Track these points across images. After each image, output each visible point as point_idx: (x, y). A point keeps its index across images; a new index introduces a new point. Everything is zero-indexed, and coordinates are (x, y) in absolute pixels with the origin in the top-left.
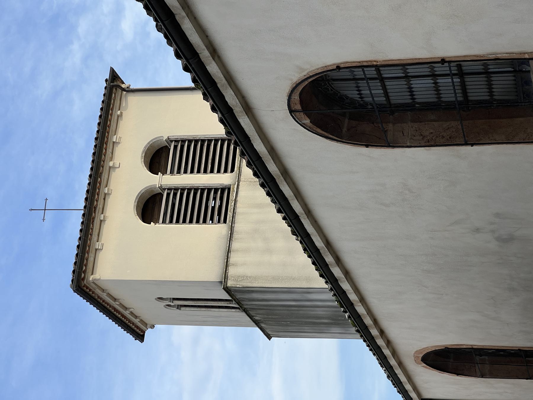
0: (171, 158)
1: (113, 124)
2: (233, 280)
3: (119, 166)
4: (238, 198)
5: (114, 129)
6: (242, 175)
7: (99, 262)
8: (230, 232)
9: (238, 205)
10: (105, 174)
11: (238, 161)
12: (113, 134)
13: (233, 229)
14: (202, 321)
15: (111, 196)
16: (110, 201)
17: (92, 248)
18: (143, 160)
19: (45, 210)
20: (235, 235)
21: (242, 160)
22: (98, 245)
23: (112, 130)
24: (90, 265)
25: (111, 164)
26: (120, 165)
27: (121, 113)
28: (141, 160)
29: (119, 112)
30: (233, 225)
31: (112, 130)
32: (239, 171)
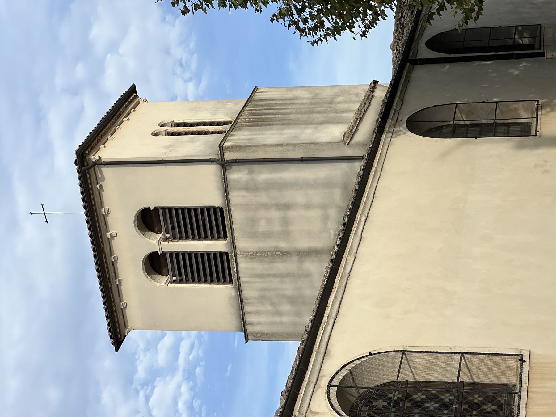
0: (162, 220)
1: (97, 199)
2: (253, 336)
3: (117, 235)
4: (239, 269)
5: (99, 203)
6: (237, 249)
7: (127, 315)
8: (240, 300)
10: (106, 246)
11: (229, 231)
12: (100, 207)
13: (241, 295)
15: (118, 261)
17: (115, 291)
18: (137, 228)
19: (45, 213)
20: (245, 301)
21: (220, 157)
23: (98, 205)
24: (121, 322)
25: (108, 235)
26: (116, 234)
27: (101, 186)
28: (135, 228)
29: (98, 186)
30: (241, 293)
31: (98, 205)
32: (234, 247)
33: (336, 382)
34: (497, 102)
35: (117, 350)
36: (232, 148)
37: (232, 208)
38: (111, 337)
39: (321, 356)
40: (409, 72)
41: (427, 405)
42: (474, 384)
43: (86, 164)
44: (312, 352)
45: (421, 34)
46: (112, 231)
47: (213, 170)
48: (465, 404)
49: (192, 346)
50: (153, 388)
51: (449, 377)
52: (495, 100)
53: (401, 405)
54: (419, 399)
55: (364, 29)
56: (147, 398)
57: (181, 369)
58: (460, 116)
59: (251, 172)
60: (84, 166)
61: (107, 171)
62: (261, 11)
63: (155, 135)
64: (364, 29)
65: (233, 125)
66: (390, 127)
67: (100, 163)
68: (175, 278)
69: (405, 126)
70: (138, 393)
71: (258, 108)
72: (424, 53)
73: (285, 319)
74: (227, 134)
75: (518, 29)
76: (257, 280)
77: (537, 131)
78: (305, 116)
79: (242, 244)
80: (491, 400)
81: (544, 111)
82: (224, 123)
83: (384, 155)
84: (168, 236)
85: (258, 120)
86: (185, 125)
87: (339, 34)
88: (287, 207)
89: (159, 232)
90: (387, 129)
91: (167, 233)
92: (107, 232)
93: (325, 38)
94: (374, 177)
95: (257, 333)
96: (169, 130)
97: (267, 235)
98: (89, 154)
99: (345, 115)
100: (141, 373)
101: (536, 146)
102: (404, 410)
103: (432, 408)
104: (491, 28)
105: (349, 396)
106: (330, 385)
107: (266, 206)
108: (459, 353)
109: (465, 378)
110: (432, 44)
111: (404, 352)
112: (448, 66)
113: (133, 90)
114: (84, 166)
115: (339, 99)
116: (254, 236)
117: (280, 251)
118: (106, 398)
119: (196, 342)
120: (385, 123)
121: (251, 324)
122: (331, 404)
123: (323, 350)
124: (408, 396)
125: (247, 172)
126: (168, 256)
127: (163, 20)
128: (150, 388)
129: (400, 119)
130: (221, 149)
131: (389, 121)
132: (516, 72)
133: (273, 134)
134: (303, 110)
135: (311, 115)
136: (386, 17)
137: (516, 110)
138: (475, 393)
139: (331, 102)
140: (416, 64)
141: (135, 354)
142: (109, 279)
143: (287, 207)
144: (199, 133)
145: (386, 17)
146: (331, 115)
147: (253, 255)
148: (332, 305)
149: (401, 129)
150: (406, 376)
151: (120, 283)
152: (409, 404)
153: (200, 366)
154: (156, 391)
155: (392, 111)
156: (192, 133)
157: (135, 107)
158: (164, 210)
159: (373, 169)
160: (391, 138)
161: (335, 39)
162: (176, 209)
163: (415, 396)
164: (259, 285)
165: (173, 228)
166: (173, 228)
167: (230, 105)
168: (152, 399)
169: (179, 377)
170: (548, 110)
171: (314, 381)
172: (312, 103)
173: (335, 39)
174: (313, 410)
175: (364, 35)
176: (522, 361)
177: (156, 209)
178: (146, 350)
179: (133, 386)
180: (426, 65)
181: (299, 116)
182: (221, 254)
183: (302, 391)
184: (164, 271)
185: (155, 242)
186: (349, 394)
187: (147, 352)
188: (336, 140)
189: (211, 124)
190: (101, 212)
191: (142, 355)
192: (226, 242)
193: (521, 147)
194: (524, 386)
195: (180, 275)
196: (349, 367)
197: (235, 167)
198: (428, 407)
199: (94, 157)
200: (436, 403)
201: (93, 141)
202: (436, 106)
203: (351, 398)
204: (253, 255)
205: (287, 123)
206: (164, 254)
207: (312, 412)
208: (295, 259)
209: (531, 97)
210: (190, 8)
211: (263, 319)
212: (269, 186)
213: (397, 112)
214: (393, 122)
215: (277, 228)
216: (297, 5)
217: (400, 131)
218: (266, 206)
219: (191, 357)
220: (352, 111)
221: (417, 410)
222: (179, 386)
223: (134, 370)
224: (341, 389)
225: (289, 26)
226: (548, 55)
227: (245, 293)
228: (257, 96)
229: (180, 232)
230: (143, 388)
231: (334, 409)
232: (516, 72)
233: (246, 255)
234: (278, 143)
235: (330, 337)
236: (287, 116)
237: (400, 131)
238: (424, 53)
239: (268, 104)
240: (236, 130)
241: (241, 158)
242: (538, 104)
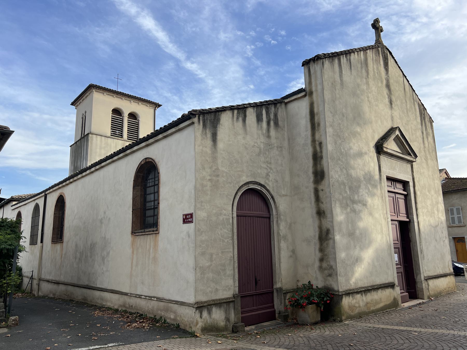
9: (117, 140)
16: (120, 100)
20: (106, 138)
22: (105, 94)
25: (132, 101)
27: (148, 107)
29: (148, 106)
46: (133, 103)
73: (98, 150)
95: (92, 138)
151: (113, 97)
160: (195, 255)
208: (225, 305)
211: (99, 142)
233: (124, 144)
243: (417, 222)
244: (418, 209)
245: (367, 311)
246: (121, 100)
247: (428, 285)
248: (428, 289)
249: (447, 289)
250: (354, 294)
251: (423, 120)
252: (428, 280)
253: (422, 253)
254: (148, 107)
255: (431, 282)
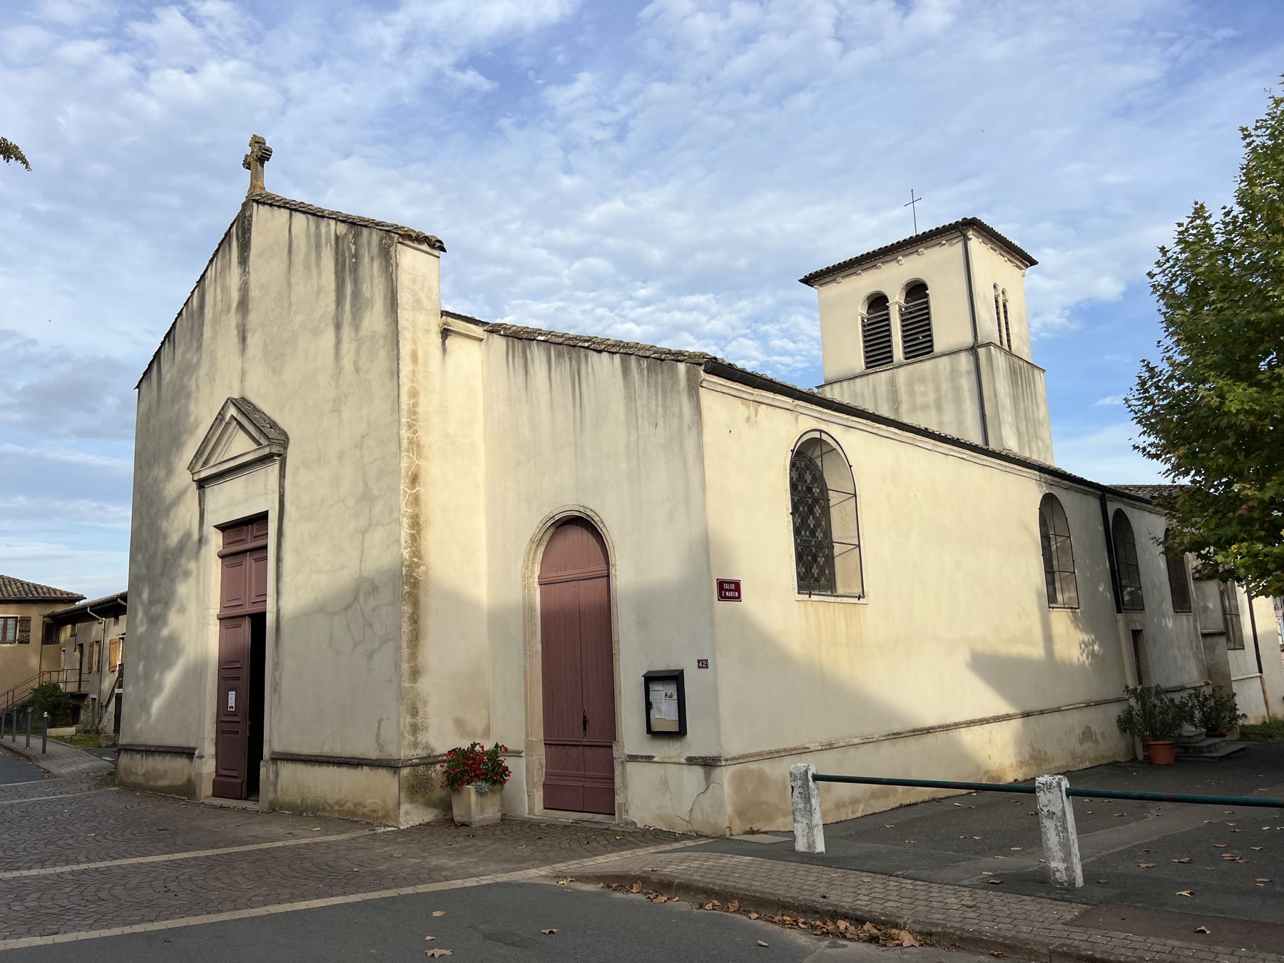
4: (879, 373)
9: (874, 375)
14: (551, 386)
16: (854, 278)
20: (852, 381)
22: (840, 279)
24: (824, 281)
27: (945, 244)
33: (824, 437)
34: (1074, 572)
35: (801, 281)
36: (989, 354)
37: (933, 361)
38: (811, 274)
39: (845, 423)
40: (1093, 494)
41: (811, 517)
42: (833, 558)
43: (964, 228)
44: (848, 414)
45: (1126, 504)
47: (968, 340)
48: (816, 550)
49: (788, 366)
50: (752, 339)
51: (836, 535)
52: (1076, 571)
53: (809, 495)
54: (815, 511)
55: (1141, 447)
56: (744, 336)
57: (770, 359)
58: (1060, 540)
59: (968, 373)
60: (962, 226)
61: (959, 247)
62: (1158, 346)
63: (995, 287)
64: (1141, 447)
65: (1009, 353)
66: (1045, 478)
67: (966, 239)
68: (866, 320)
69: (1047, 492)
70: (749, 327)
71: (1026, 374)
72: (1112, 507)
74: (1000, 348)
75: (1138, 590)
76: (871, 389)
77: (1053, 608)
78: (1023, 416)
79: (902, 374)
80: (822, 572)
81: (1071, 614)
82: (1009, 346)
83: (1020, 473)
84: (903, 309)
85: (1015, 374)
86: (1005, 312)
87: (1137, 423)
88: (939, 407)
89: (906, 302)
90: (1043, 475)
91: (906, 308)
92: (903, 256)
93: (1132, 410)
94: (1001, 465)
96: (999, 298)
97: (912, 394)
98: (973, 229)
99: (1027, 450)
100: (763, 328)
101: (1041, 607)
102: (805, 498)
103: (809, 522)
104: (1137, 566)
105: (812, 449)
106: (821, 431)
107: (938, 389)
108: (859, 543)
109: (837, 549)
110: (1119, 513)
111: (855, 495)
112: (1101, 528)
113: (1033, 263)
114: (962, 226)
115: (1040, 444)
116: (910, 383)
117: (898, 406)
118: (743, 303)
119: (791, 368)
120: (1049, 474)
121: (832, 389)
122: (806, 433)
123: (850, 424)
124: (816, 501)
125: (969, 369)
126: (886, 312)
127: (1064, 308)
128: (751, 336)
129: (1052, 487)
130: (989, 344)
131: (1050, 477)
132: (1101, 589)
133: (1005, 388)
134: (1028, 413)
135: (1024, 420)
136: (1163, 463)
137: (1069, 590)
138: (825, 558)
139: (1037, 437)
140: (1101, 501)
141: (778, 321)
142: (862, 264)
143: (939, 407)
144: (999, 324)
145: (1163, 463)
146: (1026, 438)
147: (892, 383)
148: (889, 431)
149: (1044, 489)
150: (834, 498)
152: (810, 502)
153: (772, 374)
154: (750, 342)
155: (1059, 480)
156: (999, 319)
157: (1017, 266)
158: (927, 302)
159: (1007, 464)
161: (1132, 420)
162: (928, 313)
163: (817, 507)
164: (866, 392)
165: (910, 313)
166: (910, 313)
167: (1026, 350)
168: (744, 339)
169: (763, 358)
170: (1072, 618)
171: (823, 418)
172: (1034, 420)
173: (1132, 420)
174: (799, 417)
175: (1135, 447)
176: (859, 598)
177: (927, 295)
178: (781, 330)
179: (753, 324)
180: (1100, 510)
181: (1022, 410)
182: (891, 357)
183: (814, 407)
184: (871, 311)
185: (897, 299)
186: (814, 449)
187: (779, 331)
188: (1004, 444)
189: (1008, 335)
190: (919, 248)
191: (778, 327)
192: (902, 360)
193: (1039, 594)
194: (839, 599)
195: (869, 325)
196: (838, 448)
197: (972, 358)
198: (809, 518)
199: (970, 234)
200: (814, 525)
201: (985, 232)
202: (1067, 519)
203: (810, 451)
204: (892, 383)
205: (1015, 399)
206: (887, 308)
207: (797, 416)
209: (1082, 602)
210: (1154, 279)
212: (957, 390)
213: (1058, 484)
214: (1049, 481)
215: (919, 401)
216: (1162, 382)
217: (1042, 488)
218: (938, 389)
219: (779, 366)
220: (1031, 454)
221: (806, 509)
222: (755, 359)
223: (764, 323)
224: (818, 442)
225: (1140, 377)
226: (1120, 616)
227: (858, 381)
228: (1036, 372)
229: (907, 320)
230: (752, 331)
231: (802, 436)
232: (1101, 589)
234: (998, 393)
235: (861, 430)
236: (1021, 399)
237: (1042, 488)
238: (1112, 507)
239: (1030, 383)
240: (1005, 356)
241: (981, 363)
242: (1076, 608)
243: (275, 610)
244: (282, 575)
245: (144, 784)
246: (877, 270)
247: (277, 775)
248: (275, 785)
249: (349, 805)
250: (134, 753)
251: (347, 273)
252: (279, 762)
253: (275, 690)
254: (945, 244)
255: (287, 770)
